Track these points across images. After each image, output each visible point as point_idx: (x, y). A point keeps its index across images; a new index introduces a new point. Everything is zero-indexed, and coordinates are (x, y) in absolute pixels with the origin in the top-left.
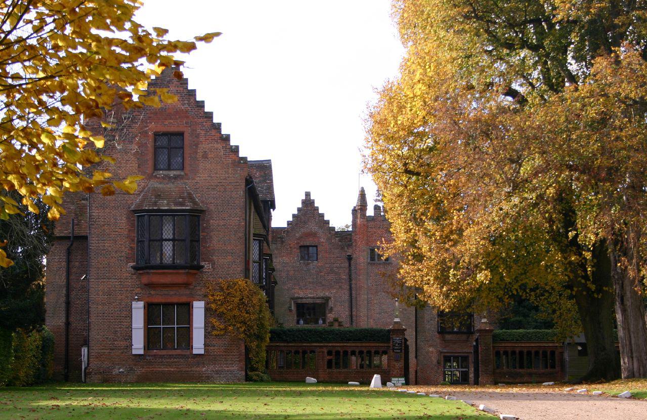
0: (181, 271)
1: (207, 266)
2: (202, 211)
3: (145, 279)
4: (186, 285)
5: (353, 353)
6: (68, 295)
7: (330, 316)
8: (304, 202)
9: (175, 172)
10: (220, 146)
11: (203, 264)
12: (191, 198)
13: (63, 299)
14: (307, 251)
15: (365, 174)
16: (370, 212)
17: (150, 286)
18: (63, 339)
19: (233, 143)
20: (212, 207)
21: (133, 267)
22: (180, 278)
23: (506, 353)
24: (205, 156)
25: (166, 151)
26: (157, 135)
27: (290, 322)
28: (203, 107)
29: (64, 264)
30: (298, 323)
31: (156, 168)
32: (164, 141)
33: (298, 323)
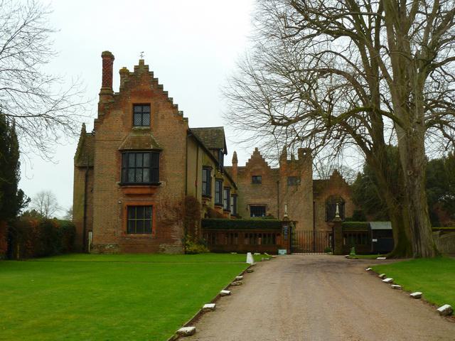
0: (146, 186)
1: (163, 183)
2: (161, 150)
3: (126, 191)
4: (150, 195)
5: (260, 236)
6: (86, 201)
7: (268, 213)
8: (254, 153)
9: (145, 128)
10: (171, 111)
11: (161, 182)
12: (154, 142)
13: (83, 204)
14: (256, 181)
15: (46, 75)
16: (289, 158)
17: (129, 195)
18: (83, 226)
19: (180, 109)
20: (166, 148)
21: (119, 184)
22: (148, 191)
23: (355, 235)
24: (163, 118)
25: (140, 115)
26: (135, 105)
27: (247, 216)
28: (162, 88)
29: (84, 182)
30: (252, 216)
31: (134, 125)
32: (139, 109)
33: (252, 216)
